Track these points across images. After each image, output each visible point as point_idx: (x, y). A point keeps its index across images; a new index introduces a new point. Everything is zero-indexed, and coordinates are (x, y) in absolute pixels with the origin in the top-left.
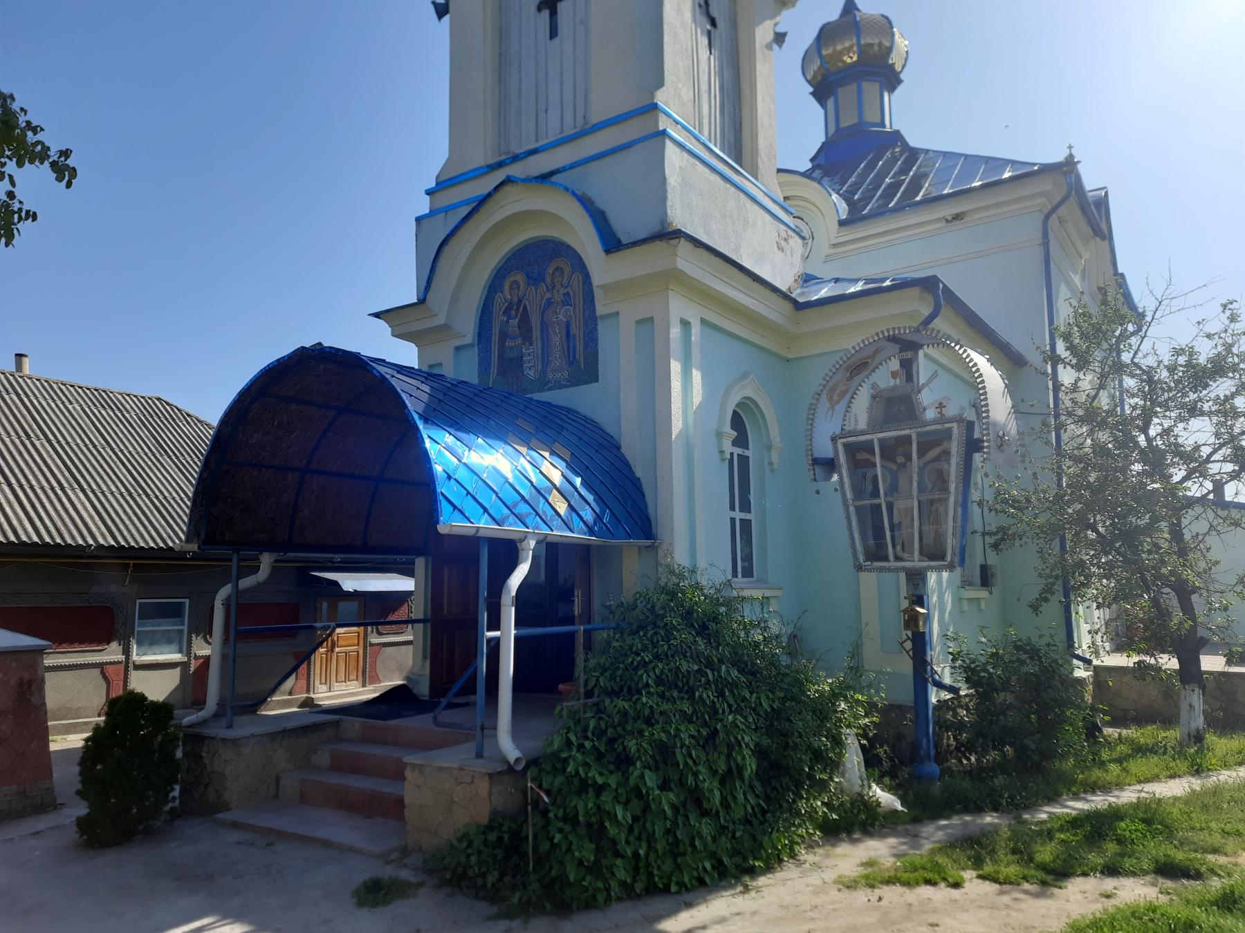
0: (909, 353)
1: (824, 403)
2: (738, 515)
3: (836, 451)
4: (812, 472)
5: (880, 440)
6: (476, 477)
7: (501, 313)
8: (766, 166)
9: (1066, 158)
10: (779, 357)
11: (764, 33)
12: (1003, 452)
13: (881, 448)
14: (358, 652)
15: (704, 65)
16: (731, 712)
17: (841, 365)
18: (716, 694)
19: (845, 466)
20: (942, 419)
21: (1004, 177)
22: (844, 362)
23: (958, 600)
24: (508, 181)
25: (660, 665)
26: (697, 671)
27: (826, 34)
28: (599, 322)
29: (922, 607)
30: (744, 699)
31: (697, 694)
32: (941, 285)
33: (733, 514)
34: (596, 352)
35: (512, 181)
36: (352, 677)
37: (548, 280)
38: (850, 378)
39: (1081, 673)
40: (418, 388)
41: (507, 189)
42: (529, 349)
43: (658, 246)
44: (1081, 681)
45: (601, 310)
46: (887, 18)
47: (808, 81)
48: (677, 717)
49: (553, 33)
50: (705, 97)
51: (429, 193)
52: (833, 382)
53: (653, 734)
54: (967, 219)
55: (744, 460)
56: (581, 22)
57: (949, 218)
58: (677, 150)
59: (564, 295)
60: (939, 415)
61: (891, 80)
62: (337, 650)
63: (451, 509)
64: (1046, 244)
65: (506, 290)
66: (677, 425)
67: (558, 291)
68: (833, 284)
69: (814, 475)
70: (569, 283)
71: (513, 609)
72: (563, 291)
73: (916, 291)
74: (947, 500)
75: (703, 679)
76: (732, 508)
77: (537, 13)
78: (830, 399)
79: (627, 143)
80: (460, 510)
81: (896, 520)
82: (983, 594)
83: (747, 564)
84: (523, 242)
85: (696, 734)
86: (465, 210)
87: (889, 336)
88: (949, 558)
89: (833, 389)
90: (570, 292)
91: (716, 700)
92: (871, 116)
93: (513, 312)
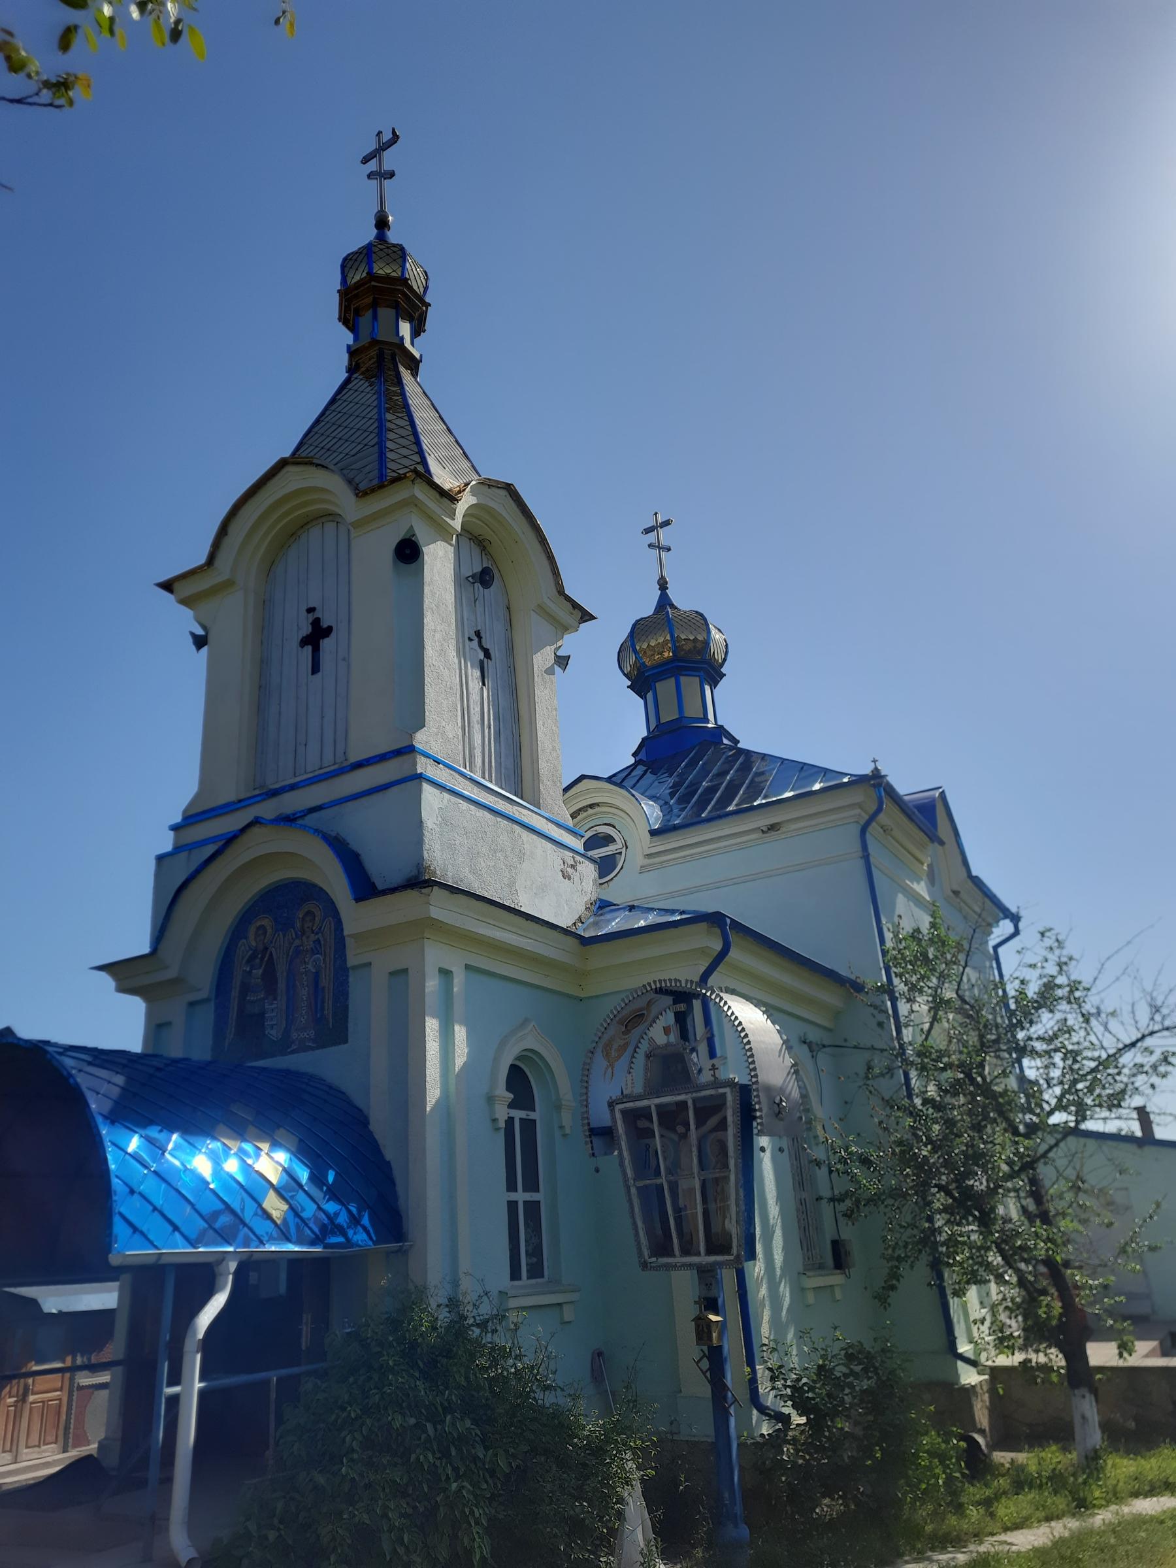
0: (682, 1005)
1: (600, 1062)
2: (521, 1196)
3: (614, 1119)
4: (590, 1145)
5: (657, 1106)
6: (164, 1186)
7: (244, 961)
8: (551, 792)
9: (872, 771)
10: (576, 998)
11: (543, 658)
12: (782, 1120)
13: (659, 1115)
14: (60, 1400)
15: (475, 696)
16: (458, 1477)
17: (612, 1020)
18: (438, 1455)
19: (623, 1137)
20: (717, 1083)
21: (814, 789)
22: (615, 1016)
23: (799, 1291)
24: (256, 822)
25: (368, 1421)
26: (415, 1425)
27: (639, 629)
28: (351, 972)
29: (717, 1313)
30: (475, 1459)
31: (413, 1457)
32: (728, 921)
33: (513, 1196)
34: (347, 1007)
35: (260, 823)
36: (50, 1438)
37: (298, 924)
38: (627, 1031)
39: (970, 1377)
40: (109, 1082)
41: (256, 830)
42: (272, 1004)
43: (411, 894)
44: (970, 1391)
45: (352, 960)
46: (701, 615)
47: (624, 674)
48: (387, 1490)
49: (315, 669)
50: (477, 728)
51: (175, 828)
52: (606, 1037)
53: (355, 1516)
54: (783, 829)
55: (529, 1126)
56: (344, 659)
57: (765, 829)
58: (436, 791)
59: (314, 942)
60: (713, 1079)
61: (713, 674)
62: (31, 1398)
63: (129, 1231)
64: (866, 857)
65: (251, 936)
66: (433, 1093)
67: (308, 937)
68: (627, 913)
69: (592, 1148)
70: (320, 929)
71: (199, 1356)
72: (313, 937)
73: (703, 926)
74: (727, 1178)
75: (423, 1436)
76: (511, 1186)
77: (300, 648)
78: (607, 1055)
79: (384, 785)
80: (142, 1233)
81: (681, 1203)
82: (836, 1279)
83: (535, 1260)
84: (274, 883)
85: (409, 1511)
86: (210, 850)
87: (656, 988)
88: (735, 1251)
89: (608, 1046)
90: (321, 939)
91: (438, 1463)
92: (692, 711)
93: (258, 961)
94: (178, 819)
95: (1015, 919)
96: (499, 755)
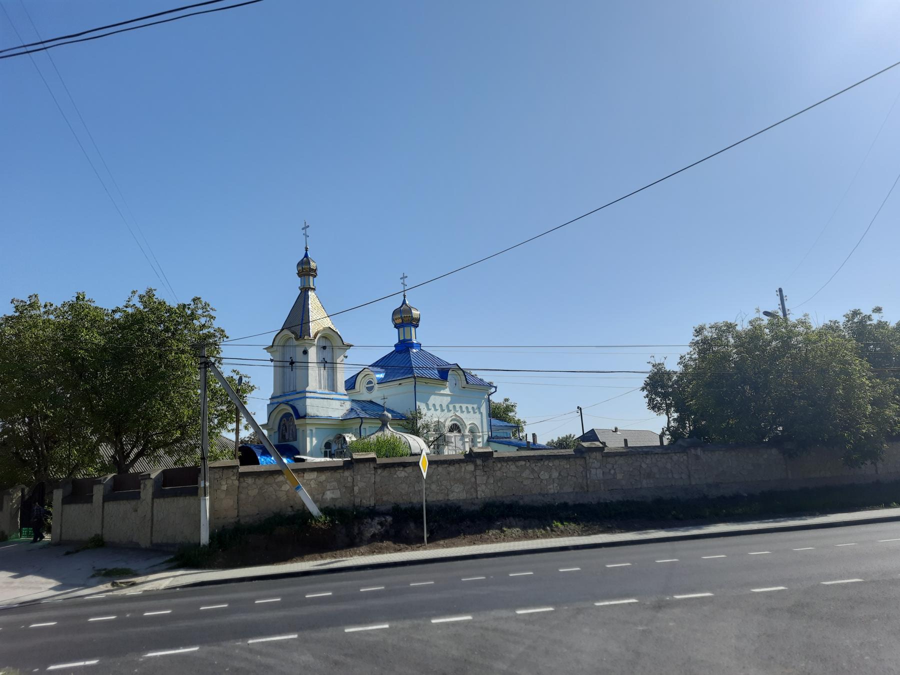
94: (270, 397)
95: (496, 387)
96: (328, 383)
